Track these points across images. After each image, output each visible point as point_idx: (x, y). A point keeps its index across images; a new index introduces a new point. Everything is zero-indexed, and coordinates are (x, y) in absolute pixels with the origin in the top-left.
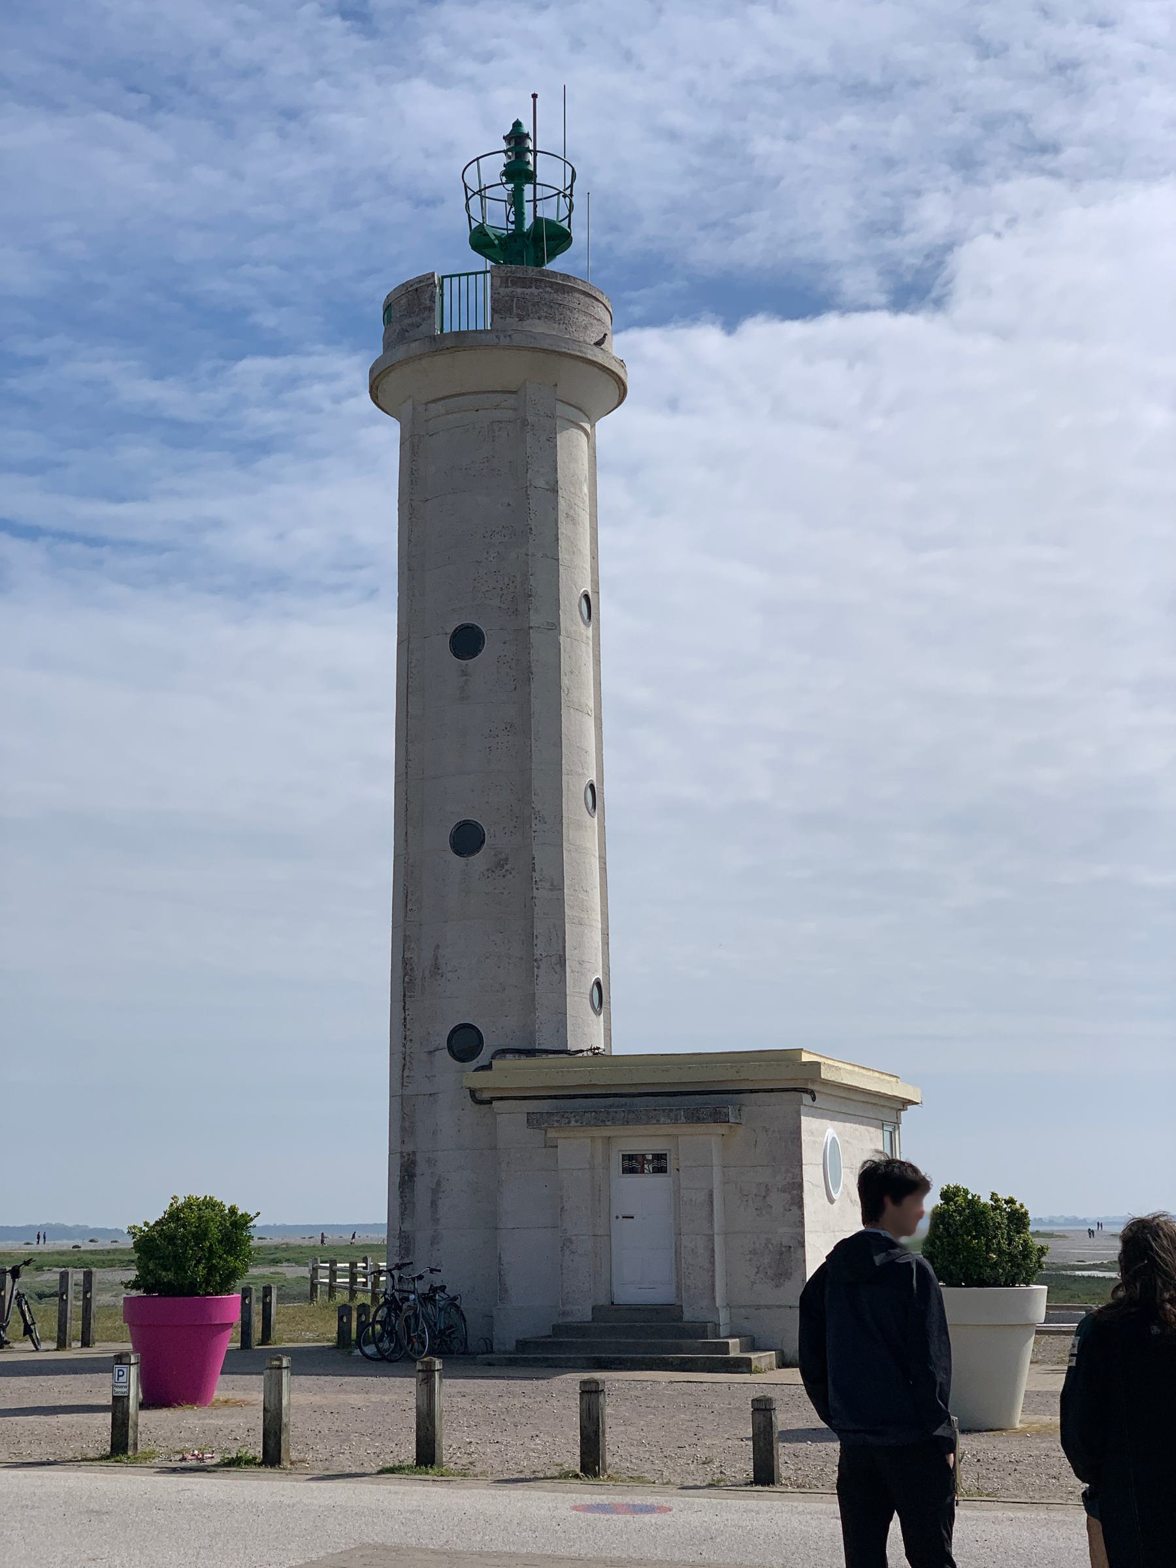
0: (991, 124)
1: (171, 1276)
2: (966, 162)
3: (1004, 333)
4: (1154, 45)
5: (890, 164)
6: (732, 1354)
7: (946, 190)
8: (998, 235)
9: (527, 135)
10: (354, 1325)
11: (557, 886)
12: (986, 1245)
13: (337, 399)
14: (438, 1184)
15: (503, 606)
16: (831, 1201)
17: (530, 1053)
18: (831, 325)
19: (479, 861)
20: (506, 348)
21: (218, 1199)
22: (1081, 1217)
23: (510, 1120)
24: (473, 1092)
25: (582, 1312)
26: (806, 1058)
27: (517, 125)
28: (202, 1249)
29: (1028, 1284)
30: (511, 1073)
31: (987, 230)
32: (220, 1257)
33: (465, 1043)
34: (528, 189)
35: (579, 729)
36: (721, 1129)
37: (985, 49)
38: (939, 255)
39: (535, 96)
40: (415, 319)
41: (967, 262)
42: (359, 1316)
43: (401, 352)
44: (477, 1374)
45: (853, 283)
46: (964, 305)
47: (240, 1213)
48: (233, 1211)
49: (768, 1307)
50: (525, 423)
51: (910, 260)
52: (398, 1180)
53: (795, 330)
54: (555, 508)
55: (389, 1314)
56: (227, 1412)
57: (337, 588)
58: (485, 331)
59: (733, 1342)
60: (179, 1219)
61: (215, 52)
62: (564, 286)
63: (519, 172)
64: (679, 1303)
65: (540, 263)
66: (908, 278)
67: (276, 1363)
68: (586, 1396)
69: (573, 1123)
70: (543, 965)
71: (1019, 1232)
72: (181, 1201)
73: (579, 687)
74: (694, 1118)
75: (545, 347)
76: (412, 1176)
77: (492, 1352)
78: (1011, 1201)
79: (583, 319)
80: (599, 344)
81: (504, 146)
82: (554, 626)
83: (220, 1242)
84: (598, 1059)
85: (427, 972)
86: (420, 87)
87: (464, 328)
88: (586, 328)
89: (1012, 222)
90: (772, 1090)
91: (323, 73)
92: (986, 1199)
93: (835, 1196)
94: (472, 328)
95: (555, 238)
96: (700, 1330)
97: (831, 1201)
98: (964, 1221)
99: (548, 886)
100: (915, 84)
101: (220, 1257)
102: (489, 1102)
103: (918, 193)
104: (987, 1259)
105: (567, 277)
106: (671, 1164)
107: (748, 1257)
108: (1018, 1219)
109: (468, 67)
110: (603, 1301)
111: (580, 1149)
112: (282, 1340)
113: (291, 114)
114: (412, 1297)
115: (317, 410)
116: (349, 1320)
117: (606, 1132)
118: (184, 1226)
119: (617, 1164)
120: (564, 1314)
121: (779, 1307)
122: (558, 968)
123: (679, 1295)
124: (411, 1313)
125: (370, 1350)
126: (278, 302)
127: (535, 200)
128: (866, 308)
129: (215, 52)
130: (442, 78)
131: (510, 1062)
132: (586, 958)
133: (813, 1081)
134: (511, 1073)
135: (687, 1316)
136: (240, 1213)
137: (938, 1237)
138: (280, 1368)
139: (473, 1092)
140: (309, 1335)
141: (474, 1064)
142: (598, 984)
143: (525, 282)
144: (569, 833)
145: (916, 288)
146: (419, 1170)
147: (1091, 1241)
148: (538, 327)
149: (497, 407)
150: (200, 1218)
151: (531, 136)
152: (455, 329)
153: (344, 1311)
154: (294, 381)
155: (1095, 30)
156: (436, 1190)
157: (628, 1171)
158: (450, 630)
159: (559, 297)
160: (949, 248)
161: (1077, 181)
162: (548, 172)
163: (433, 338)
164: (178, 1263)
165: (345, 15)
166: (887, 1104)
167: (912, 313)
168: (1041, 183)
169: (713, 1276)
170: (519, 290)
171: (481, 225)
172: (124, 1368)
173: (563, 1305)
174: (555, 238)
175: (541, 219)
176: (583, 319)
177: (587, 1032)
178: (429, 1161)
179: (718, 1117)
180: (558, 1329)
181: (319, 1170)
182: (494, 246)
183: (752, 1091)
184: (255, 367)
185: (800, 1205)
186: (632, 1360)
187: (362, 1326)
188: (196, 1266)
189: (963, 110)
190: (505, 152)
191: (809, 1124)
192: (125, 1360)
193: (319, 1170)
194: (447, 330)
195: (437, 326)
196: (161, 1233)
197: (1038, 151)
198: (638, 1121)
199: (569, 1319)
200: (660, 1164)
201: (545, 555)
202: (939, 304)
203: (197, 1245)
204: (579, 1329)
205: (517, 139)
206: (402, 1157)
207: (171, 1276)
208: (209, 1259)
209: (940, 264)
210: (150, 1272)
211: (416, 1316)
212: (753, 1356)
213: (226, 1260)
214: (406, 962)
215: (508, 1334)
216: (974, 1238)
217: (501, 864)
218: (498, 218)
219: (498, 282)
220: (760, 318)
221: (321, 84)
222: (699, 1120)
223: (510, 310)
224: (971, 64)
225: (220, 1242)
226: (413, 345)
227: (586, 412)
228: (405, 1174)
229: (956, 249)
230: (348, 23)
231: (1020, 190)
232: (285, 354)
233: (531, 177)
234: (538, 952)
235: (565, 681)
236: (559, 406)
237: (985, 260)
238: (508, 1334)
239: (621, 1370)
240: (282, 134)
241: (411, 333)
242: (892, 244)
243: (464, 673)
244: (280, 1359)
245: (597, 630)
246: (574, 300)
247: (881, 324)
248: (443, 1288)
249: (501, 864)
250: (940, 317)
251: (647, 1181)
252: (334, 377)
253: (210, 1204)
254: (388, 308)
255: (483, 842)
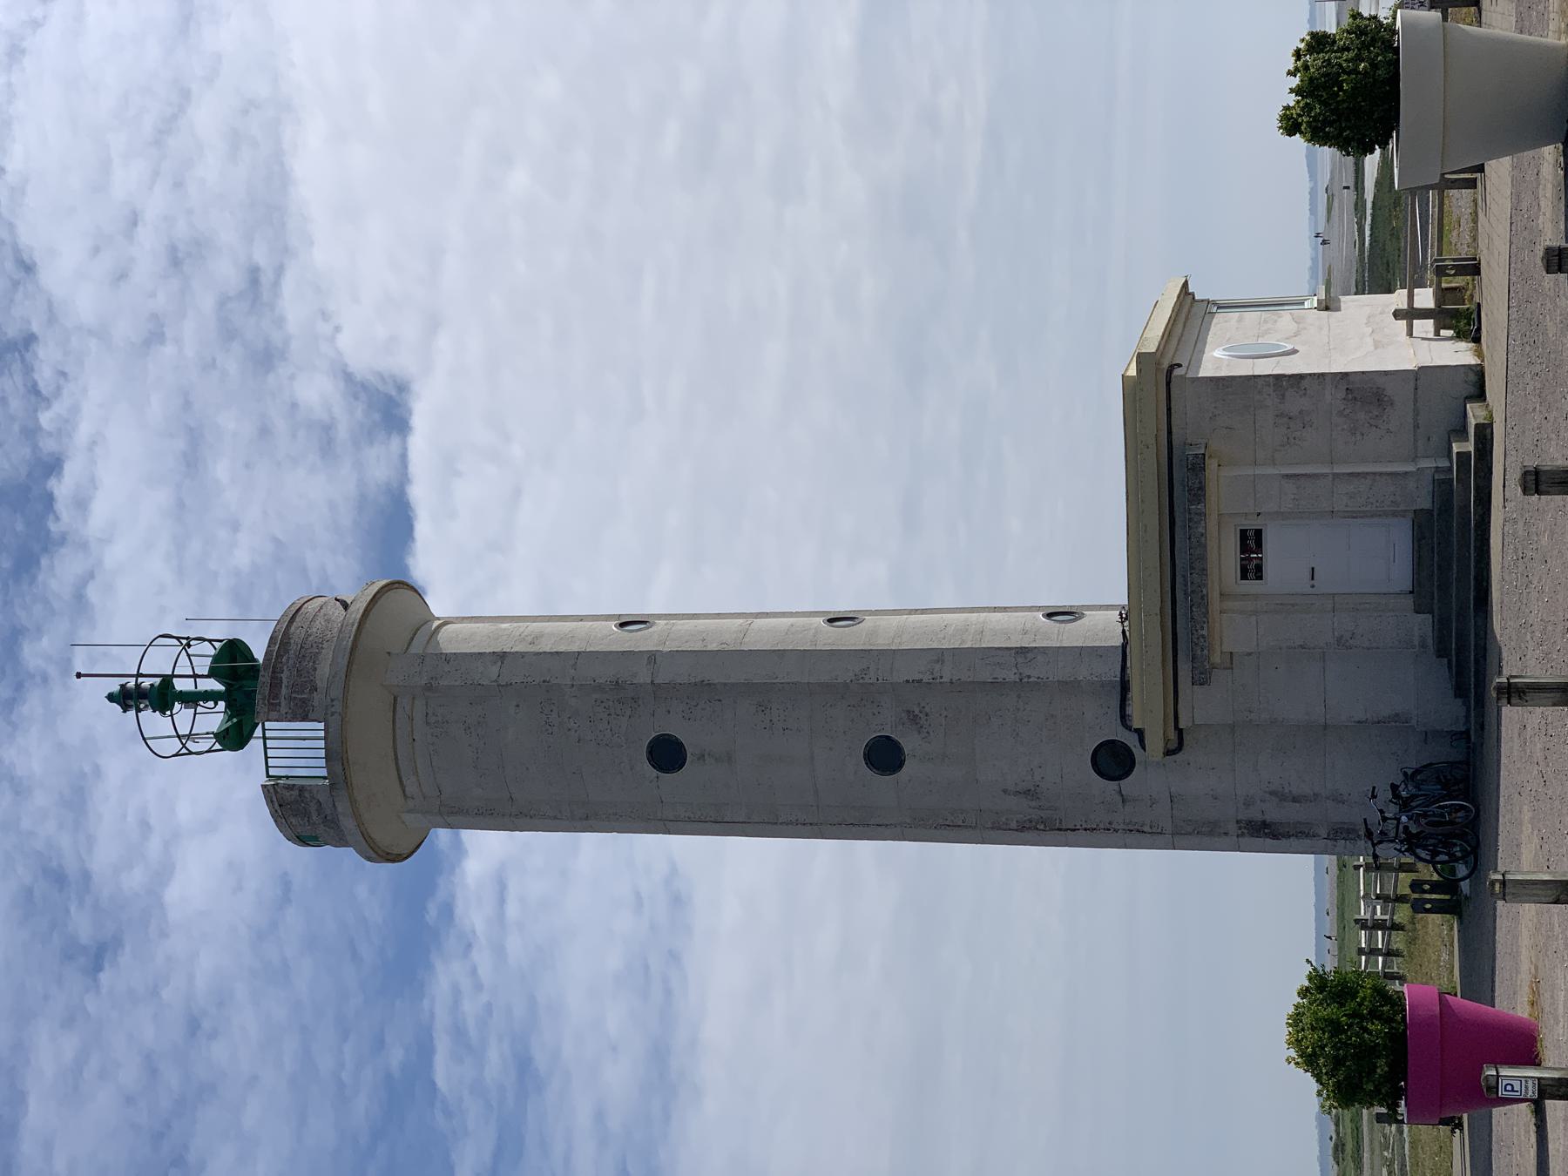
0: (228, 333)
1: (1382, 1062)
2: (266, 358)
3: (433, 324)
4: (156, 174)
5: (265, 431)
6: (1472, 449)
7: (292, 377)
8: (338, 329)
9: (123, 686)
10: (1434, 896)
11: (939, 656)
12: (1349, 74)
13: (478, 987)
14: (1272, 793)
15: (628, 712)
16: (1294, 352)
17: (1125, 687)
18: (419, 493)
19: (909, 743)
20: (345, 706)
21: (1292, 1010)
22: (1309, 263)
23: (1201, 706)
24: (1168, 753)
25: (1422, 625)
26: (1132, 372)
27: (111, 697)
28: (1350, 1026)
29: (1395, 32)
30: (1147, 708)
31: (332, 339)
32: (1360, 1005)
33: (1113, 761)
34: (181, 685)
35: (763, 635)
36: (1211, 465)
37: (155, 336)
38: (354, 386)
39: (79, 675)
40: (313, 808)
41: (362, 361)
42: (1425, 892)
43: (348, 824)
44: (1494, 721)
45: (379, 471)
46: (403, 362)
47: (1307, 983)
48: (1304, 993)
49: (1416, 412)
50: (429, 688)
51: (359, 414)
52: (1269, 841)
53: (423, 528)
54: (523, 655)
55: (1424, 848)
56: (1547, 995)
57: (668, 992)
58: (326, 730)
59: (1456, 448)
60: (1314, 1054)
61: (130, 1100)
62: (281, 642)
63: (162, 696)
64: (1411, 515)
65: (254, 670)
66: (377, 416)
67: (1497, 886)
68: (1543, 487)
69: (1204, 632)
70: (1027, 672)
71: (1334, 42)
72: (1293, 1053)
73: (723, 635)
74: (1198, 494)
75: (346, 662)
76: (1265, 824)
77: (1467, 732)
78: (1298, 54)
79: (319, 623)
80: (345, 606)
81: (132, 713)
82: (652, 657)
83: (1342, 1005)
84: (1133, 616)
85: (1033, 804)
86: (172, 894)
87: (322, 753)
88: (328, 621)
89: (325, 315)
90: (1169, 409)
91: (155, 992)
92: (1295, 81)
93: (1289, 347)
94: (322, 744)
95: (232, 657)
96: (1442, 487)
97: (1294, 352)
98: (1320, 103)
99: (937, 667)
100: (187, 405)
101: (1360, 1005)
102: (1180, 732)
103: (294, 405)
104: (1366, 72)
105: (272, 640)
106: (1252, 524)
107: (1359, 437)
108: (1318, 42)
109: (154, 846)
110: (1409, 602)
111: (1234, 626)
112: (1450, 981)
113: (193, 1026)
114: (1404, 819)
115: (489, 1008)
116: (1429, 901)
117: (1214, 596)
118: (1322, 1048)
119: (1252, 586)
120: (1423, 645)
121: (1416, 401)
122: (1030, 656)
123: (1403, 514)
124: (1423, 821)
125: (1462, 870)
126: (380, 1044)
127: (195, 676)
128: (404, 457)
129: (130, 1100)
130: (164, 873)
131: (1134, 709)
132: (1020, 627)
133: (1158, 364)
134: (1147, 708)
135: (1425, 503)
136: (1307, 983)
137: (1340, 134)
138: (1503, 883)
139: (1168, 753)
140: (1445, 957)
141: (1137, 751)
142: (1049, 615)
143: (275, 684)
144: (882, 643)
145: (388, 409)
146: (1259, 817)
147: (1334, 242)
148: (324, 670)
149: (411, 719)
150: (1313, 1029)
151: (123, 680)
152: (323, 763)
153: (1418, 907)
154: (458, 1032)
155: (140, 228)
156: (1281, 796)
157: (1259, 573)
158: (655, 772)
159: (293, 648)
160: (348, 377)
161: (286, 250)
162: (159, 662)
163: (332, 786)
164: (1366, 1053)
165: (98, 968)
166: (1185, 310)
167: (410, 412)
168: (288, 285)
169: (1381, 474)
170: (284, 691)
171: (216, 735)
172: (1502, 1083)
173: (1413, 647)
174: (232, 657)
175: (211, 669)
176: (319, 623)
177: (1103, 628)
178: (1247, 804)
179: (1197, 466)
180: (1442, 652)
181: (1259, 922)
182: (239, 724)
183: (1170, 432)
184: (443, 1071)
185: (1301, 377)
186: (1477, 562)
187: (1435, 887)
188: (1370, 1033)
189: (214, 360)
190: (139, 710)
191: (1206, 371)
192: (1492, 1082)
193: (1259, 922)
194: (324, 773)
195: (321, 782)
196: (1331, 1074)
197: (256, 288)
198: (1203, 558)
199: (1430, 641)
200: (1251, 541)
201: (574, 666)
202: (403, 387)
203: (1345, 1032)
204: (1442, 625)
205: (127, 698)
206: (1243, 835)
207: (1382, 1062)
208: (1362, 1018)
209: (364, 386)
210: (1377, 1090)
211: (1425, 815)
212: (1472, 422)
213: (1364, 999)
214: (1022, 828)
215: (1448, 712)
216: (1340, 88)
217: (913, 719)
218: (213, 718)
219: (274, 714)
220: (410, 561)
221: (166, 994)
222: (1202, 488)
223: (303, 701)
224: (169, 350)
225: (1342, 1005)
226: (340, 809)
227: (423, 624)
228: (1263, 832)
229: (350, 370)
230: (107, 965)
231: (293, 307)
232: (431, 1039)
233: (167, 680)
234: (1011, 676)
235: (713, 647)
236: (413, 650)
237: (361, 341)
238: (1448, 712)
239: (1488, 564)
240: (213, 1035)
241: (328, 812)
242: (343, 432)
243: (702, 757)
244: (1493, 883)
245: (660, 617)
246: (297, 633)
247: (419, 444)
248: (1394, 787)
249: (913, 719)
250: (415, 387)
251: (1272, 554)
252: (456, 992)
253: (1296, 1020)
254: (302, 840)
255: (888, 737)
